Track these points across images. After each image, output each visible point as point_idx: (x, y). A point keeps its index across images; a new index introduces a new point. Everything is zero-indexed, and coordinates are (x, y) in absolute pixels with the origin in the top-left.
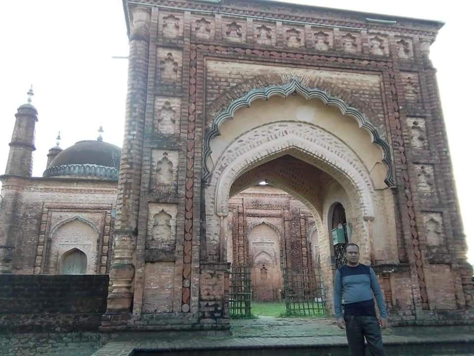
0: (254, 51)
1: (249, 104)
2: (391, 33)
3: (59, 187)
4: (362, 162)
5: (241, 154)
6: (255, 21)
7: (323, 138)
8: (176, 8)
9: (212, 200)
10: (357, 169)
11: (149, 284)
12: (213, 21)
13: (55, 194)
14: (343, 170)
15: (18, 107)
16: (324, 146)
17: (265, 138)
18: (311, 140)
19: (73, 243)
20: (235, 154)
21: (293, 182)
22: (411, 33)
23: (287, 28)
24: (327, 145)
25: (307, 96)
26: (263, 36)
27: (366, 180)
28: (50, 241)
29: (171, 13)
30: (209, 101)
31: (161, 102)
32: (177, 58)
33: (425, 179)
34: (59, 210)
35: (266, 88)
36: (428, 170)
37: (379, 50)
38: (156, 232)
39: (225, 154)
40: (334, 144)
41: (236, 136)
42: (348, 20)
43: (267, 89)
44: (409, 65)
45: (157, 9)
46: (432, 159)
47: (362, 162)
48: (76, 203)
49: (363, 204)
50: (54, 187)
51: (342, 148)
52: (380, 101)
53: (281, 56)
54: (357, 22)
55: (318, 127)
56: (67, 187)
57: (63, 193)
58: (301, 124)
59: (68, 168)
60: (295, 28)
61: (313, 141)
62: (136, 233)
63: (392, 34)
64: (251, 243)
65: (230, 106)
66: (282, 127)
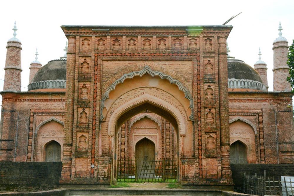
1: (123, 82)
2: (201, 35)
3: (40, 98)
4: (183, 106)
5: (121, 105)
7: (163, 94)
8: (88, 35)
9: (106, 128)
10: (179, 110)
13: (37, 103)
17: (133, 96)
19: (52, 137)
20: (118, 106)
22: (213, 34)
23: (143, 39)
24: (165, 98)
26: (132, 44)
27: (184, 115)
29: (85, 38)
31: (81, 84)
33: (211, 115)
34: (41, 114)
38: (80, 144)
39: (113, 106)
40: (168, 98)
41: (118, 97)
42: (176, 31)
43: (132, 73)
45: (79, 36)
47: (183, 106)
48: (52, 109)
50: (36, 98)
51: (173, 99)
55: (160, 89)
56: (45, 98)
57: (43, 103)
58: (151, 88)
59: (44, 83)
61: (157, 96)
62: (71, 145)
66: (141, 90)
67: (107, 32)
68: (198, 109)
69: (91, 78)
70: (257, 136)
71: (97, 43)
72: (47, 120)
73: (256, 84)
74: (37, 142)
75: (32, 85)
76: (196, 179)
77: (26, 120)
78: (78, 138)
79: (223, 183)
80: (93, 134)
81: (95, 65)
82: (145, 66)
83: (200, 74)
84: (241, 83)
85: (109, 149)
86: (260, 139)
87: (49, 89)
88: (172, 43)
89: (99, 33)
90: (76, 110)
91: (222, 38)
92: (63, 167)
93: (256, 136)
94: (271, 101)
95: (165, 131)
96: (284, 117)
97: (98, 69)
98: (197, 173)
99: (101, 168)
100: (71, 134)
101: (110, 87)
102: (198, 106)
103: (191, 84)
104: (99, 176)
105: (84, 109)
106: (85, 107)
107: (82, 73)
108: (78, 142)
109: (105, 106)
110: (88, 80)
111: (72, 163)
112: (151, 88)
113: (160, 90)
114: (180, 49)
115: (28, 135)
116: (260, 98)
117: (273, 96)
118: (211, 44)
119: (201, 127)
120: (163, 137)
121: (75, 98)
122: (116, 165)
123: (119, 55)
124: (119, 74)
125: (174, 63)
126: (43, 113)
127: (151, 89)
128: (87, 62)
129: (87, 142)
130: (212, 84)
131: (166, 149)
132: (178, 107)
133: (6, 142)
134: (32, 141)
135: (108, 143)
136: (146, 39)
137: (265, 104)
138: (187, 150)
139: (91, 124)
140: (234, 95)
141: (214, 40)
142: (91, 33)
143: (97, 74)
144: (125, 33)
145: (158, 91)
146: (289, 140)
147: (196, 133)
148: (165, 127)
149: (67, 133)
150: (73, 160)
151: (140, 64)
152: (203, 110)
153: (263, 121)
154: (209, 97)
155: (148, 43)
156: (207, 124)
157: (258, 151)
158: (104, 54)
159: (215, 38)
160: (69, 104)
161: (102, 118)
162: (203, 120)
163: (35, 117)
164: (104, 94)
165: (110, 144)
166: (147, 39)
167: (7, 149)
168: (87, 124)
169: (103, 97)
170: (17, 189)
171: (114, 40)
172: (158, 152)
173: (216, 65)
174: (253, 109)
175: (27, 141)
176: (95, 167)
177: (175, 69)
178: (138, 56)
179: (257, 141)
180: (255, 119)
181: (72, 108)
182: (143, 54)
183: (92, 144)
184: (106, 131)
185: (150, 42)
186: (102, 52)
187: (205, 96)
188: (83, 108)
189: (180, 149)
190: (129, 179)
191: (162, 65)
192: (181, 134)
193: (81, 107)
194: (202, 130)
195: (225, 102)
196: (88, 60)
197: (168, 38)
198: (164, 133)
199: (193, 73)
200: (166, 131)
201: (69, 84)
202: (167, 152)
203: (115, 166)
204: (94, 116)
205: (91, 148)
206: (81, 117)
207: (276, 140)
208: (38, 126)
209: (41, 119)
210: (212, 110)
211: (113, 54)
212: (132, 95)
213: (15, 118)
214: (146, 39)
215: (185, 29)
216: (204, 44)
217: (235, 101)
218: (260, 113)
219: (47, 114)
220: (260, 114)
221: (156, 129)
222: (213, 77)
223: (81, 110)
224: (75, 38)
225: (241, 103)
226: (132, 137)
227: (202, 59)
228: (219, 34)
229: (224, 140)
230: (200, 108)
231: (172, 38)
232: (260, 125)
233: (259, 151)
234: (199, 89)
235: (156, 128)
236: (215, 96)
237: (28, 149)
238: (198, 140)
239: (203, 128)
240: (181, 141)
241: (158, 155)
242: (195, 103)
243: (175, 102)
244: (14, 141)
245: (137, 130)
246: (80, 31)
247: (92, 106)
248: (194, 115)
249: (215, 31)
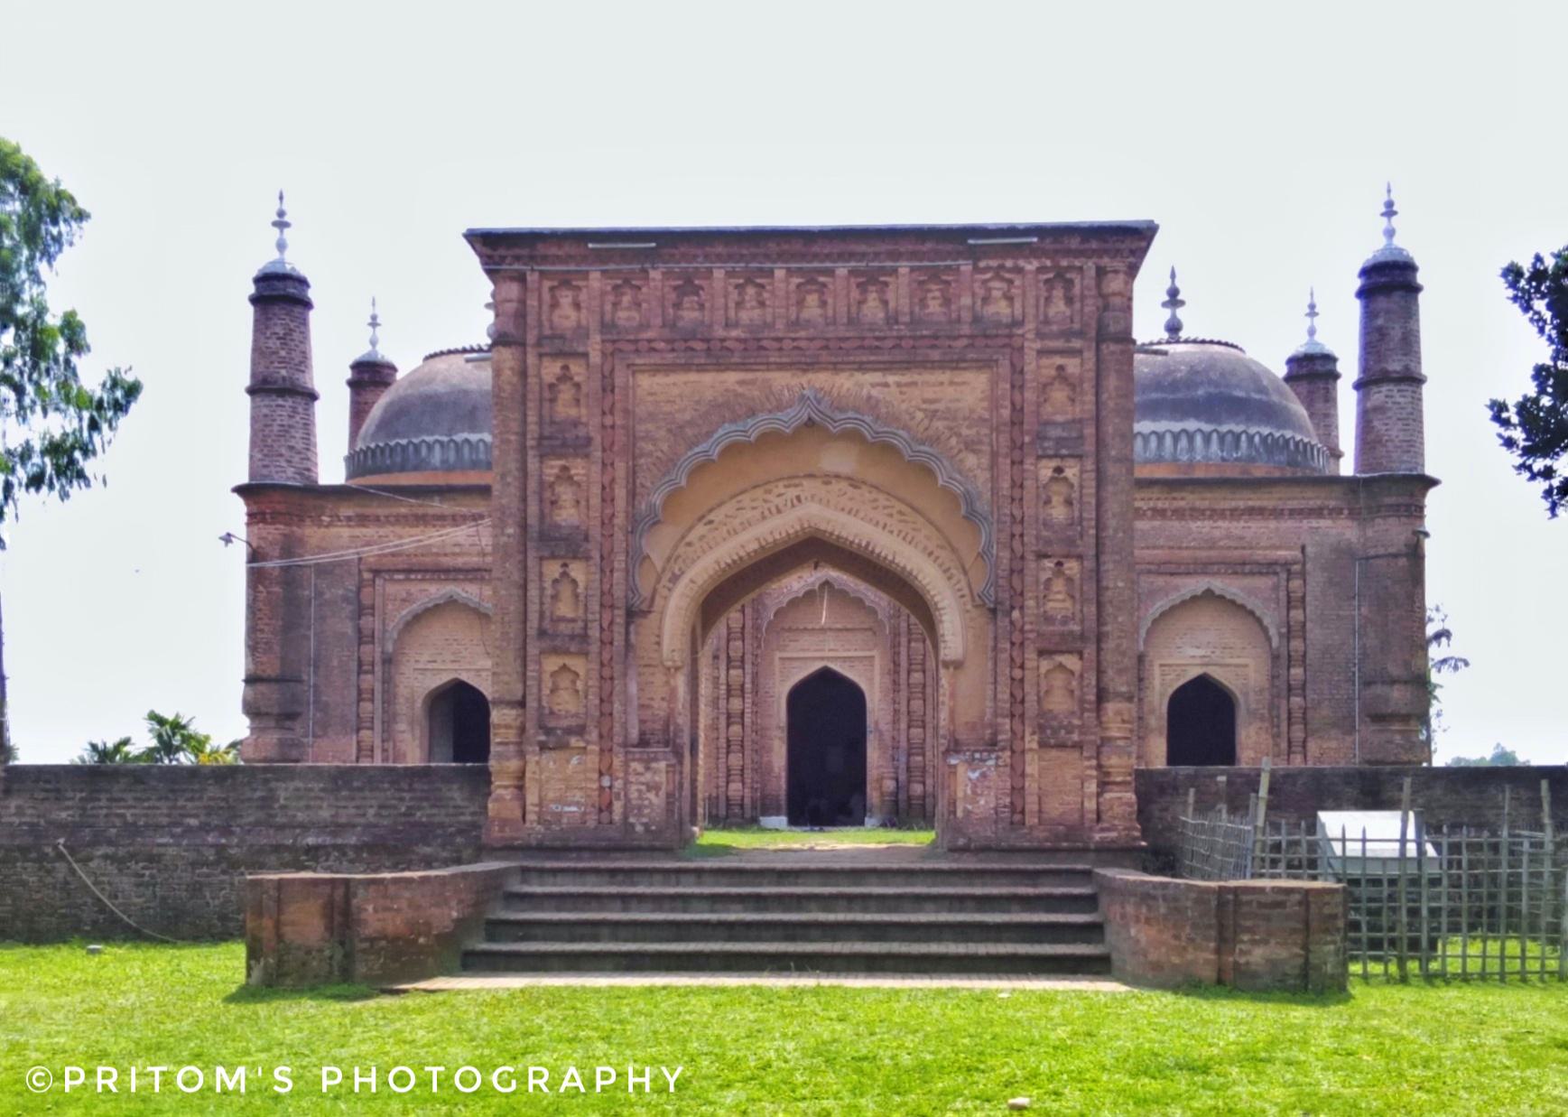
6: (730, 274)
7: (875, 505)
10: (940, 566)
15: (254, 273)
23: (796, 280)
27: (958, 586)
32: (578, 374)
34: (401, 577)
37: (1003, 303)
39: (682, 550)
40: (896, 516)
42: (929, 246)
43: (750, 422)
47: (954, 550)
48: (446, 555)
55: (864, 482)
62: (522, 704)
69: (589, 440)
71: (611, 298)
75: (362, 456)
78: (546, 677)
80: (606, 662)
81: (604, 390)
83: (1022, 423)
84: (1222, 438)
88: (911, 297)
90: (537, 569)
93: (1275, 658)
95: (904, 640)
97: (618, 406)
98: (1005, 806)
101: (667, 479)
102: (1012, 550)
103: (985, 461)
105: (565, 565)
107: (552, 423)
108: (546, 691)
112: (828, 478)
113: (864, 487)
114: (943, 319)
116: (1295, 502)
118: (1069, 301)
120: (896, 664)
123: (699, 346)
125: (916, 378)
128: (571, 379)
130: (1071, 462)
131: (909, 713)
132: (936, 554)
134: (372, 681)
139: (596, 625)
140: (1192, 493)
141: (1083, 282)
143: (613, 427)
150: (532, 759)
152: (1031, 565)
153: (1304, 597)
154: (1058, 513)
156: (1048, 619)
157: (1278, 717)
160: (506, 545)
162: (1030, 603)
164: (643, 507)
165: (672, 695)
166: (812, 281)
167: (279, 715)
168: (580, 624)
171: (675, 288)
173: (1088, 387)
174: (1266, 548)
177: (925, 401)
178: (777, 353)
183: (602, 700)
184: (656, 647)
186: (632, 337)
189: (944, 715)
191: (873, 385)
192: (948, 658)
194: (1027, 643)
195: (1121, 535)
196: (577, 369)
198: (903, 651)
200: (909, 642)
205: (597, 714)
208: (392, 625)
209: (404, 595)
210: (1066, 566)
211: (676, 345)
214: (808, 282)
215: (965, 240)
216: (1042, 301)
217: (1195, 514)
218: (1295, 563)
221: (870, 633)
222: (1074, 434)
223: (553, 569)
224: (521, 279)
225: (1220, 523)
227: (1030, 363)
229: (1112, 680)
230: (1022, 558)
231: (914, 275)
232: (1293, 613)
233: (1284, 716)
234: (1018, 483)
235: (870, 629)
240: (946, 686)
246: (541, 249)
247: (596, 555)
249: (1086, 246)
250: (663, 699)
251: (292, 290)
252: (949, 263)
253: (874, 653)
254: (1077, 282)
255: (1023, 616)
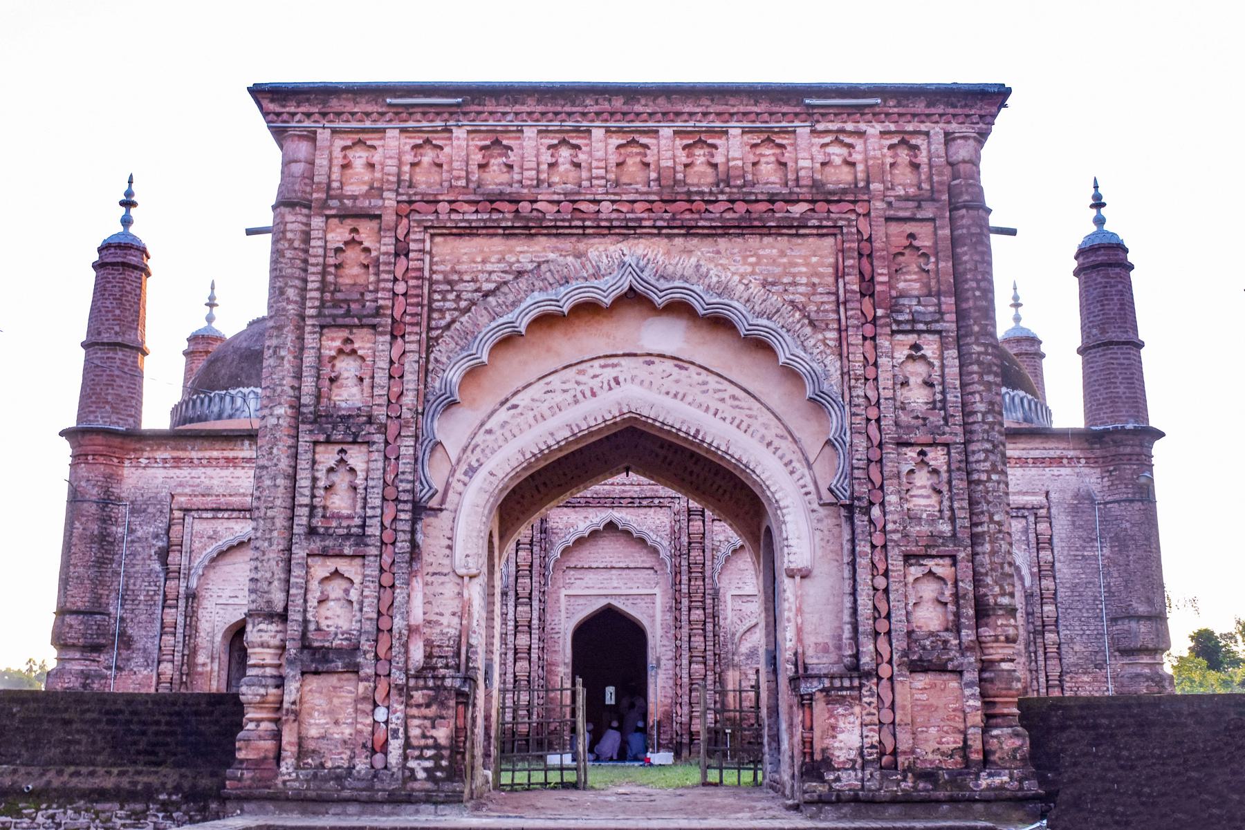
0: (537, 206)
1: (522, 329)
2: (873, 127)
3: (208, 454)
7: (705, 388)
10: (781, 458)
11: (310, 715)
12: (447, 142)
14: (744, 462)
16: (704, 408)
18: (675, 396)
21: (691, 473)
22: (923, 122)
23: (616, 141)
25: (659, 301)
27: (802, 482)
28: (192, 596)
29: (357, 137)
30: (437, 328)
34: (210, 515)
35: (562, 288)
36: (936, 459)
38: (323, 611)
39: (479, 438)
40: (730, 402)
41: (502, 398)
43: (563, 290)
44: (911, 204)
46: (944, 433)
47: (795, 441)
49: (787, 539)
50: (194, 455)
51: (750, 409)
52: (833, 298)
53: (599, 211)
54: (785, 109)
55: (692, 363)
57: (218, 470)
59: (228, 399)
60: (637, 137)
61: (680, 396)
62: (283, 617)
63: (874, 129)
64: (729, 598)
65: (480, 336)
66: (609, 370)
67: (453, 111)
68: (868, 448)
70: (1032, 595)
71: (409, 158)
72: (232, 538)
73: (1022, 400)
74: (194, 619)
76: (868, 772)
77: (157, 536)
78: (314, 585)
79: (989, 788)
80: (386, 567)
82: (626, 259)
85: (460, 636)
86: (1042, 605)
87: (242, 419)
89: (419, 116)
90: (309, 455)
91: (965, 138)
92: (244, 720)
94: (1079, 462)
95: (685, 578)
96: (1127, 521)
98: (872, 746)
99: (419, 726)
100: (281, 564)
101: (465, 354)
104: (412, 764)
106: (350, 439)
109: (439, 437)
110: (365, 321)
111: (286, 698)
112: (650, 357)
113: (692, 367)
115: (162, 592)
116: (1038, 452)
117: (1086, 445)
118: (915, 166)
119: (884, 530)
121: (302, 401)
122: (494, 713)
124: (505, 294)
126: (219, 510)
127: (650, 363)
129: (355, 604)
133: (81, 617)
134: (175, 616)
135: (456, 610)
136: (629, 143)
137: (1056, 473)
138: (820, 640)
139: (376, 521)
142: (382, 114)
144: (536, 116)
145: (684, 372)
146: (1146, 605)
147: (863, 562)
148: (684, 563)
149: (262, 561)
150: (292, 688)
151: (602, 251)
152: (890, 452)
153: (1051, 539)
155: (638, 159)
157: (1035, 653)
158: (441, 204)
159: (934, 139)
161: (424, 494)
162: (892, 499)
163: (190, 526)
165: (464, 612)
167: (84, 647)
169: (432, 398)
170: (51, 811)
171: (482, 148)
172: (658, 660)
175: (160, 616)
176: (393, 718)
179: (1033, 614)
180: (1022, 532)
181: (290, 447)
182: (615, 207)
183: (379, 613)
184: (448, 552)
185: (646, 155)
187: (898, 393)
188: (338, 448)
190: (549, 773)
192: (792, 566)
193: (328, 442)
197: (724, 138)
199: (841, 291)
201: (277, 337)
202: (694, 659)
203: (487, 718)
204: (390, 483)
206: (328, 488)
207: (1102, 609)
212: (565, 391)
213: (114, 528)
214: (629, 143)
218: (1041, 508)
219: (235, 514)
220: (1043, 512)
221: (652, 571)
223: (328, 457)
224: (311, 137)
226: (558, 600)
228: (949, 122)
231: (746, 137)
232: (1042, 554)
234: (871, 361)
236: (943, 393)
237: (160, 647)
238: (872, 593)
239: (896, 537)
240: (792, 599)
241: (659, 671)
242: (857, 420)
243: (761, 420)
244: (109, 615)
245: (577, 574)
246: (335, 104)
248: (853, 478)
249: (933, 110)
250: (454, 614)
251: (133, 260)
252: (784, 124)
253: (657, 591)
254: (924, 147)
255: (884, 513)
